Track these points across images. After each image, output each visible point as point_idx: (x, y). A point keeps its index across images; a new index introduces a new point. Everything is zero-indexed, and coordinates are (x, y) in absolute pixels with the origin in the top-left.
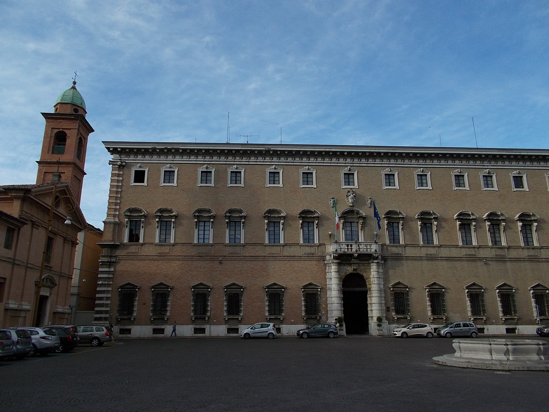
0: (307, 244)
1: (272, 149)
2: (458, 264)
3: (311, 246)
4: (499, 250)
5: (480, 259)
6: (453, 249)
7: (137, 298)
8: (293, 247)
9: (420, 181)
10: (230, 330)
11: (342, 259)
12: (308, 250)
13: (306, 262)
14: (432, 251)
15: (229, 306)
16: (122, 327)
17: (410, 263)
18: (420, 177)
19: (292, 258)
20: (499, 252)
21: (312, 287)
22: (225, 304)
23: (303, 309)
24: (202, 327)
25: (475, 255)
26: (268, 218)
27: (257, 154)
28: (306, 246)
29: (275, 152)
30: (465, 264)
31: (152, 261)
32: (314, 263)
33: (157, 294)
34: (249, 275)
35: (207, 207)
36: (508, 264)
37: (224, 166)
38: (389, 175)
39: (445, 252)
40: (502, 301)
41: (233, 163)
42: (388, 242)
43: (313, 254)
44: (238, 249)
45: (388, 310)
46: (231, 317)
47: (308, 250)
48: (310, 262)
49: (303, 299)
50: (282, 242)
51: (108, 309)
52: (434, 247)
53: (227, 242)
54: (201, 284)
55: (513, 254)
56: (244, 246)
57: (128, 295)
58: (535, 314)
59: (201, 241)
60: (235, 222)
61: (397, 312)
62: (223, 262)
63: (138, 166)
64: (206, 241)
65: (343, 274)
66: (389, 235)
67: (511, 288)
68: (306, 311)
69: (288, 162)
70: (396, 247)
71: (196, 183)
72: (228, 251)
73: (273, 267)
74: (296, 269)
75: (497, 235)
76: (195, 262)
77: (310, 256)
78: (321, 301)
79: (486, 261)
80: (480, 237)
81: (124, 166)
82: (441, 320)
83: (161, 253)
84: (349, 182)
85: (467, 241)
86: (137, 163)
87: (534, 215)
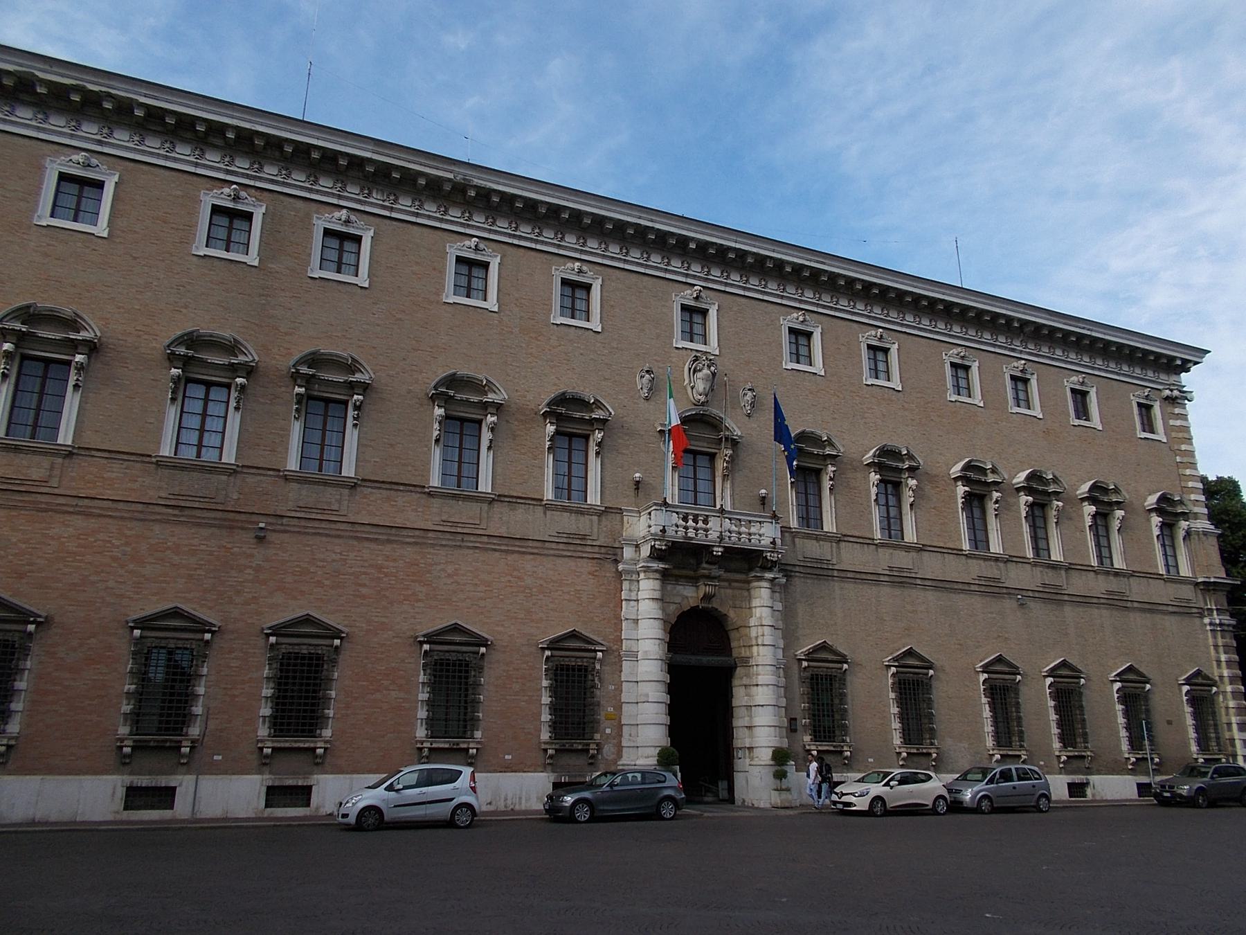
4: (1050, 573)
5: (1011, 592)
10: (275, 795)
13: (559, 561)
14: (903, 560)
17: (851, 589)
18: (568, 291)
22: (267, 692)
23: (546, 717)
24: (163, 781)
28: (565, 509)
29: (485, 195)
32: (586, 566)
34: (364, 591)
37: (300, 204)
41: (335, 201)
43: (584, 537)
44: (330, 496)
46: (442, 744)
49: (545, 683)
53: (293, 464)
54: (176, 613)
61: (816, 738)
62: (272, 537)
64: (329, 470)
66: (556, 474)
71: (187, 238)
73: (450, 569)
74: (529, 581)
76: (157, 528)
77: (575, 544)
78: (602, 693)
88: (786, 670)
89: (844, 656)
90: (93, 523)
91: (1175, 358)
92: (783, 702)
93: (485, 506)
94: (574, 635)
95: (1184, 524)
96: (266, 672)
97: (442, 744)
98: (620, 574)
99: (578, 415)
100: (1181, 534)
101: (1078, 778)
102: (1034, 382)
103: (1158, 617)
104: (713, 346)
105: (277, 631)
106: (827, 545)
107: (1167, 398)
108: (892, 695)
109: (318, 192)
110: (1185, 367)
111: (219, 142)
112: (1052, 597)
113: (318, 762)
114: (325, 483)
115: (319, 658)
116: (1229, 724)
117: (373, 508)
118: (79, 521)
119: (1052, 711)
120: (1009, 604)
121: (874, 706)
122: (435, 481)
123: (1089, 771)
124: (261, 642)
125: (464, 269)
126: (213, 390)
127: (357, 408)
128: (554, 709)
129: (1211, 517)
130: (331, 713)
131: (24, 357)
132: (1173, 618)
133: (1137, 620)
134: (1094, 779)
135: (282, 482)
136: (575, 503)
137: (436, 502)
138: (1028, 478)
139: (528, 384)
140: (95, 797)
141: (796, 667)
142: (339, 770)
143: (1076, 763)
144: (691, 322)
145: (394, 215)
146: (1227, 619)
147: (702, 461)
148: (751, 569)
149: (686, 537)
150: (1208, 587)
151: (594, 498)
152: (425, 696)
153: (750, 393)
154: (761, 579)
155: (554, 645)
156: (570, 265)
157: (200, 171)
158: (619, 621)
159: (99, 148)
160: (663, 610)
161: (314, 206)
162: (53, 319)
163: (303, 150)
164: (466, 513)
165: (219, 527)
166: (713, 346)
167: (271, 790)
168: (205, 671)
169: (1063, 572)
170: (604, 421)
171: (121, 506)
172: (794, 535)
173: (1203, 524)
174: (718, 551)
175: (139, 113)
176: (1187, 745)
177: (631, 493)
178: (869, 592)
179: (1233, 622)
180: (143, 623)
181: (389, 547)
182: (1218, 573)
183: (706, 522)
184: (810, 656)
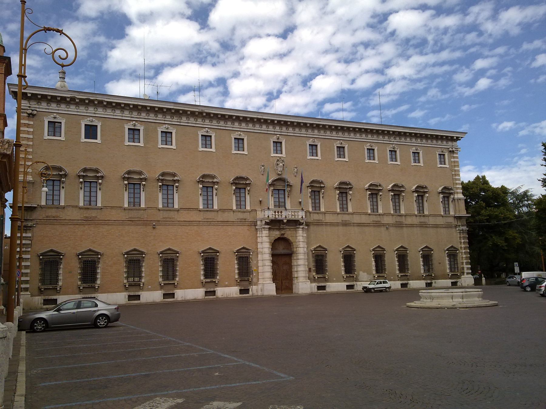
0: (240, 210)
1: (106, 100)
2: (367, 229)
3: (244, 212)
4: (399, 217)
5: (384, 225)
6: (363, 217)
7: (62, 266)
8: (226, 213)
9: (237, 145)
10: (165, 296)
11: (274, 224)
12: (241, 216)
13: (238, 227)
14: (346, 218)
15: (205, 270)
16: (47, 298)
17: (329, 228)
18: (204, 138)
19: (225, 223)
20: (399, 219)
21: (245, 251)
22: (161, 269)
23: (237, 271)
24: (137, 294)
25: (380, 221)
26: (236, 184)
27: (188, 115)
28: (239, 212)
29: (208, 114)
30: (372, 229)
31: (77, 226)
32: (246, 228)
33: (85, 261)
34: (184, 240)
35: (137, 169)
36: (405, 229)
37: (153, 124)
38: (166, 132)
39: (356, 219)
40: (398, 261)
41: (163, 122)
42: (311, 210)
43: (245, 219)
44: (172, 214)
45: (310, 270)
46: (167, 282)
47: (241, 216)
48: (242, 227)
49: (236, 262)
50: (216, 207)
51: (28, 279)
52: (349, 214)
53: (160, 206)
54: (135, 250)
55: (409, 221)
56: (178, 211)
57: (51, 263)
58: (422, 271)
59: (50, 203)
60: (168, 185)
61: (317, 273)
62: (157, 227)
63: (52, 116)
64: (56, 203)
65: (273, 239)
66: (236, 201)
67: (384, 250)
68: (239, 274)
69: (52, 109)
70: (318, 213)
71: (123, 141)
72: (160, 216)
73: (207, 232)
74: (230, 233)
75: (317, 201)
76: (127, 227)
77: (243, 222)
78: (253, 263)
79: (387, 226)
80: (385, 205)
81: (34, 115)
82: (352, 278)
83: (87, 217)
84: (206, 144)
85: (374, 208)
86: (50, 112)
87: (380, 185)
88: (308, 254)
89: (60, 253)
90: (110, 227)
91: (453, 137)
92: (307, 263)
93: (216, 213)
94: (244, 248)
95: (452, 196)
96: (160, 264)
97: (208, 280)
98: (257, 229)
99: (242, 182)
100: (451, 200)
101: (429, 281)
102: (398, 152)
103: (439, 229)
104: (284, 155)
105: (162, 253)
106: (321, 215)
107: (450, 151)
108: (342, 260)
109: (158, 120)
110: (458, 139)
111: (128, 108)
112: (399, 225)
113: (175, 286)
114: (170, 210)
115: (139, 260)
116: (463, 263)
117: (184, 216)
118: (106, 227)
119: (421, 262)
120: (383, 229)
121: (335, 262)
122: (201, 207)
123: (408, 280)
124: (158, 256)
125: (131, 132)
126: (135, 185)
127: (177, 187)
128: (239, 269)
129: (463, 194)
130: (178, 274)
131: (85, 182)
132: (445, 229)
133: (431, 231)
134: (410, 282)
135: (158, 211)
136: (137, 207)
137: (202, 213)
138: (392, 187)
139: (225, 175)
140: (199, 293)
141: (311, 253)
142: (181, 289)
143: (404, 278)
144: (276, 146)
145: (181, 124)
146: (465, 228)
147: (317, 193)
148: (296, 225)
149: (275, 218)
150: (459, 218)
151: (248, 208)
152: (161, 269)
153: (296, 169)
154: (299, 228)
155: (238, 251)
156: (237, 133)
157: (123, 118)
158: (257, 243)
159: (94, 115)
160: (269, 239)
161: (157, 124)
162: (91, 170)
163: (223, 116)
164: (210, 215)
165: (143, 225)
166: (284, 155)
167: (129, 296)
168: (144, 265)
169: (404, 217)
170: (178, 181)
171: (116, 222)
172: (310, 213)
173: (461, 196)
174: (285, 221)
175: (105, 103)
176: (446, 270)
177: (259, 204)
178: (335, 229)
179: (467, 229)
180: (127, 253)
181: (189, 227)
182: (464, 213)
183: (281, 213)
184: (315, 250)
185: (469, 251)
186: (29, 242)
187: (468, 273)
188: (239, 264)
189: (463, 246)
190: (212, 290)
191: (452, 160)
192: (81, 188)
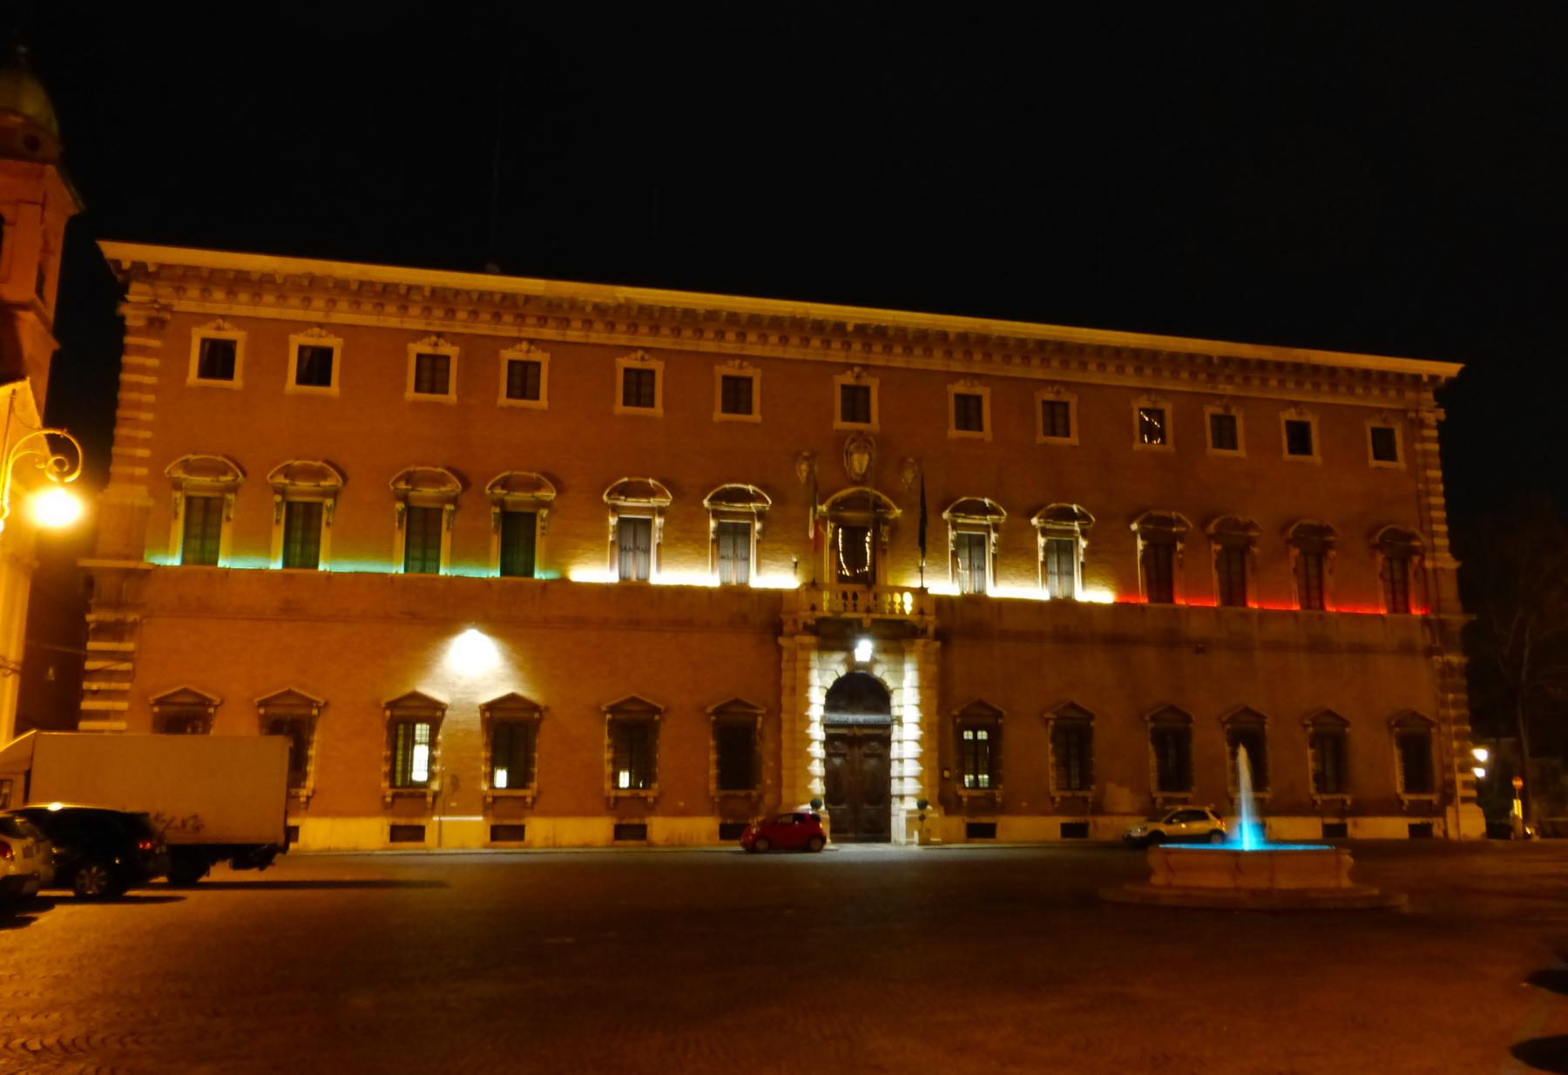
81: (163, 323)
107: (1411, 420)
146: (1455, 659)
185: (1468, 728)
186: (126, 666)
187: (1465, 800)
188: (720, 749)
189: (1453, 713)
190: (636, 821)
191: (1418, 446)
192: (278, 522)
